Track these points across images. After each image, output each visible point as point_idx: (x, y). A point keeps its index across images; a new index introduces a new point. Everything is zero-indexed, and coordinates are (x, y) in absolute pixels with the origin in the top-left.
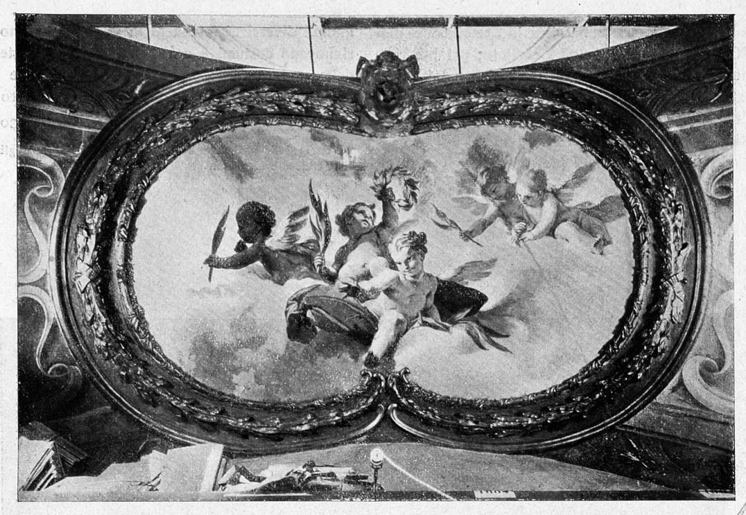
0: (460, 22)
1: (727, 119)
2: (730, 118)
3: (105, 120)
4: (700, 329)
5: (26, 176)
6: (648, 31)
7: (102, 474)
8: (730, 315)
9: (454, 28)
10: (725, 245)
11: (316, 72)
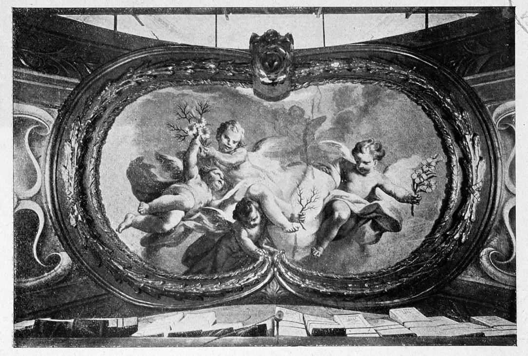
0: (326, 10)
1: (511, 79)
2: (513, 78)
3: (77, 81)
4: (49, 142)
5: (19, 124)
6: (456, 17)
7: (138, 329)
8: (513, 212)
9: (321, 15)
10: (508, 165)
11: (118, 30)
